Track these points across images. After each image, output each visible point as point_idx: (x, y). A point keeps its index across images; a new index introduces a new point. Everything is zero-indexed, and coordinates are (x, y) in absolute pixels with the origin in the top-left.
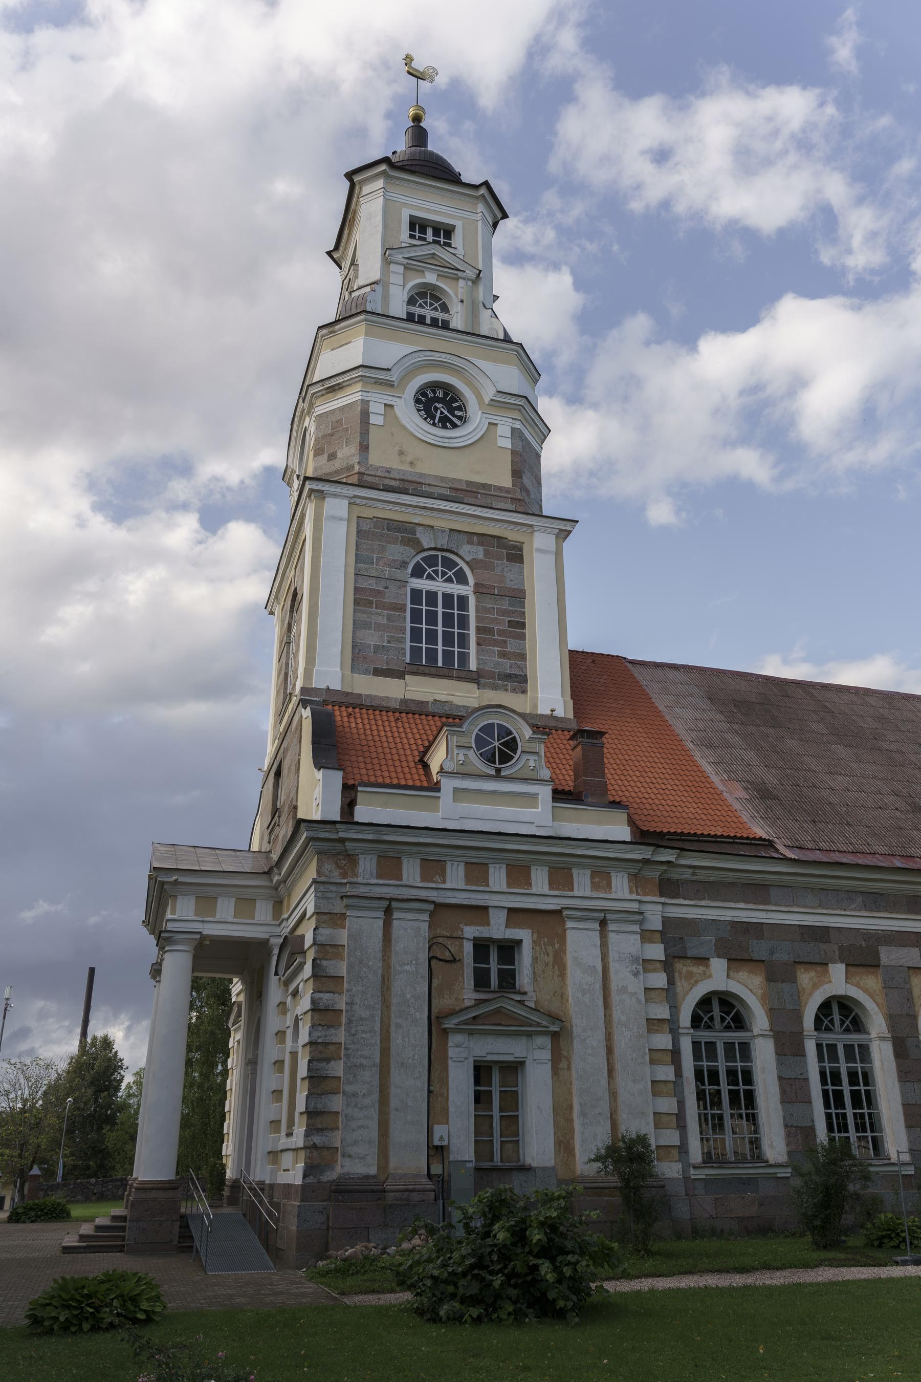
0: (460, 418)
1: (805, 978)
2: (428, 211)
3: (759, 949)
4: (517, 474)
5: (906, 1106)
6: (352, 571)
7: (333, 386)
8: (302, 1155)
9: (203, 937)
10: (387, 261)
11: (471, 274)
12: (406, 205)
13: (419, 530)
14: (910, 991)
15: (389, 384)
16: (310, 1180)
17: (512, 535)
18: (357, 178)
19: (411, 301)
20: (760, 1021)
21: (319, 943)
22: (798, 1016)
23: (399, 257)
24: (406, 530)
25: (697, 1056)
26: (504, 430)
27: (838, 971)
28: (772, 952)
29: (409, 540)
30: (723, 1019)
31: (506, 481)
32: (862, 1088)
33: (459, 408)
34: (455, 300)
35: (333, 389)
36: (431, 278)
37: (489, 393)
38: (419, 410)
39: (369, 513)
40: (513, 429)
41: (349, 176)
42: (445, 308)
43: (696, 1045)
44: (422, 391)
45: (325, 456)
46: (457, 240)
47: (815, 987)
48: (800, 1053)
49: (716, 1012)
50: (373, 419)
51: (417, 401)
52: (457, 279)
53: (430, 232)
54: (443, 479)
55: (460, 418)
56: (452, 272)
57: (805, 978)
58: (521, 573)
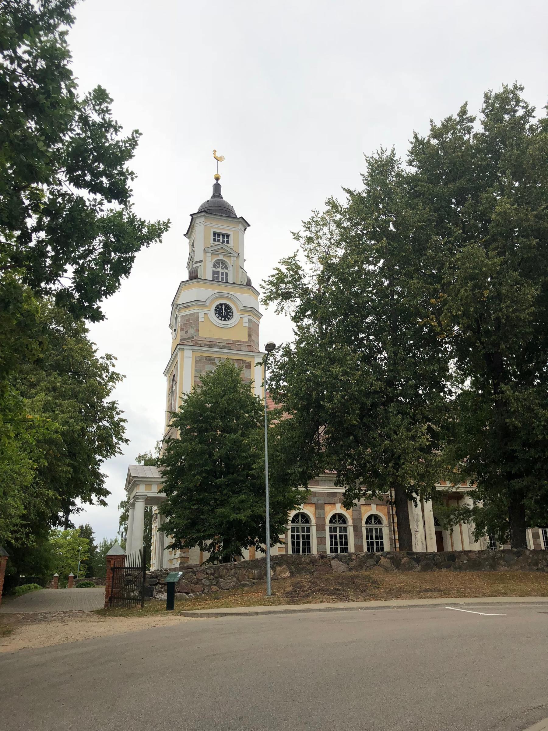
0: (230, 316)
1: (327, 508)
2: (220, 229)
3: (314, 500)
4: (249, 336)
5: (436, 531)
6: (194, 375)
7: (187, 306)
8: (179, 559)
9: (148, 497)
10: (205, 252)
11: (236, 255)
12: (213, 227)
13: (216, 359)
14: (361, 511)
15: (206, 306)
16: (181, 565)
17: (247, 359)
18: (194, 216)
19: (214, 266)
20: (313, 521)
21: (179, 358)
22: (324, 519)
23: (210, 250)
24: (211, 360)
25: (331, 531)
26: (246, 320)
27: (338, 505)
28: (318, 501)
29: (213, 363)
30: (302, 521)
31: (246, 339)
32: (369, 534)
33: (230, 312)
34: (230, 265)
35: (187, 307)
36: (221, 257)
37: (241, 307)
38: (216, 314)
39: (199, 354)
40: (249, 319)
41: (191, 215)
42: (226, 268)
43: (331, 528)
44: (217, 307)
45: (184, 331)
46: (231, 240)
47: (331, 510)
48: (324, 530)
49: (300, 519)
50: (201, 319)
51: (216, 310)
52: (231, 257)
53: (221, 237)
54: (224, 340)
55: (230, 316)
56: (229, 254)
57: (327, 508)
58: (250, 372)
